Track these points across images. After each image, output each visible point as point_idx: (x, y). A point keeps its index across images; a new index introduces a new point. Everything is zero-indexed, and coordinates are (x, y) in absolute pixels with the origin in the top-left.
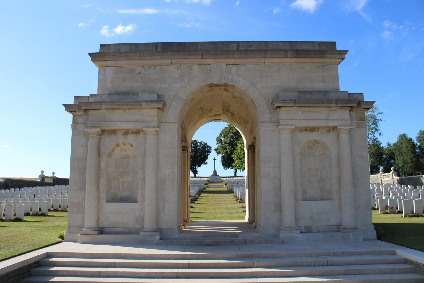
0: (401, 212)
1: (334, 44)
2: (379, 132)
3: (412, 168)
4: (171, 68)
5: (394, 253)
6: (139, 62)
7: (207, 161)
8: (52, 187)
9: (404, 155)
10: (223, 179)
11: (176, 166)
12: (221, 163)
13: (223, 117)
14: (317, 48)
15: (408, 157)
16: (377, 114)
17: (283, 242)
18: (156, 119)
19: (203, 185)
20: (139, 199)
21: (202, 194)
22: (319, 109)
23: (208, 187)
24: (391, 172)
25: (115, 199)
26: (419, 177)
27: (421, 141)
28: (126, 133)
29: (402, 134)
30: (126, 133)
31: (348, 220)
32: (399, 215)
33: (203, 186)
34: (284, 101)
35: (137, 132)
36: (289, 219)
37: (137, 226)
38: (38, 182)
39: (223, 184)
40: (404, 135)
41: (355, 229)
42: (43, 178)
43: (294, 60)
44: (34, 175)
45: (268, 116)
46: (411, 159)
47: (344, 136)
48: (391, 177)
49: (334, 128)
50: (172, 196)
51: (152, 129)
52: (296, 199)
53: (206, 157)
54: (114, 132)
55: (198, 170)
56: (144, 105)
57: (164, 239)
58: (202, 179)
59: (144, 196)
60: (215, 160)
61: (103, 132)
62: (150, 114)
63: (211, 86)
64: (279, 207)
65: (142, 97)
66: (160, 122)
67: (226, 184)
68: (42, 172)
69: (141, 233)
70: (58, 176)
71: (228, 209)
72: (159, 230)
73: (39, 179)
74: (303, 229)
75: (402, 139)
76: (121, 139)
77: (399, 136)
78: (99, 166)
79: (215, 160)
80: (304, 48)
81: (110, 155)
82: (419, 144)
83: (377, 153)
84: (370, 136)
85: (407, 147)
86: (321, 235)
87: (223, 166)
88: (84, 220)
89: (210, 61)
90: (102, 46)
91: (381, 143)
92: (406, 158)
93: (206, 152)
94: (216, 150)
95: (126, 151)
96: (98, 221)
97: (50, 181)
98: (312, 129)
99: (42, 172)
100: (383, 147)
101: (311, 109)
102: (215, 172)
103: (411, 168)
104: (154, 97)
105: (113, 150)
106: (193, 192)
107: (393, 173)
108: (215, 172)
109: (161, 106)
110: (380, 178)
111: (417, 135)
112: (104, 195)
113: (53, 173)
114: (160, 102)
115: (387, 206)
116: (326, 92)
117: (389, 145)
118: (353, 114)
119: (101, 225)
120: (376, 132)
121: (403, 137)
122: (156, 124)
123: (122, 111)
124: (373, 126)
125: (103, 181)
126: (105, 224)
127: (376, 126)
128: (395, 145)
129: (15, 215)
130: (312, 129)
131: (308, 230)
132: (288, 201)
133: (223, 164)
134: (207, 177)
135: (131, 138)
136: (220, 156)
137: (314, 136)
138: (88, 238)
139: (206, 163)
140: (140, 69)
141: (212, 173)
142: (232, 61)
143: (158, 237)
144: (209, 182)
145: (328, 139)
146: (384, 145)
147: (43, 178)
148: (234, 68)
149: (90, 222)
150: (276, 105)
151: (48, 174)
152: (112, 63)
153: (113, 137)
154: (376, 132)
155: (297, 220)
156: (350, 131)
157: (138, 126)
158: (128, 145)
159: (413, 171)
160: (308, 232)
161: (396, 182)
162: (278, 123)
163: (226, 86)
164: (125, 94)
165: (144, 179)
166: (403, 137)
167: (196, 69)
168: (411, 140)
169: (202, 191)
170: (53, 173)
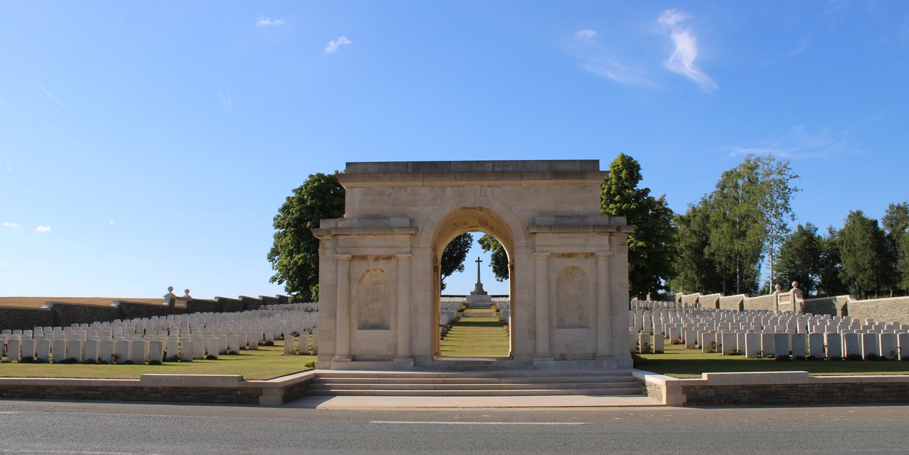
0: (700, 348)
1: (596, 163)
2: (790, 213)
3: (872, 280)
4: (424, 190)
5: (631, 374)
6: (389, 183)
7: (463, 263)
8: (186, 316)
9: (859, 254)
10: (493, 299)
11: (429, 293)
12: (491, 268)
13: (480, 228)
14: (578, 168)
15: (866, 258)
16: (788, 177)
17: (535, 369)
18: (408, 245)
19: (455, 312)
20: (392, 326)
21: (456, 329)
22: (576, 235)
23: (464, 316)
24: (792, 290)
25: (365, 327)
26: (831, 300)
27: (892, 226)
28: (377, 258)
29: (854, 211)
30: (377, 258)
31: (603, 348)
32: (698, 351)
33: (456, 314)
34: (539, 227)
35: (389, 258)
36: (543, 346)
37: (390, 353)
38: (164, 306)
39: (492, 310)
40: (859, 213)
41: (610, 357)
42: (172, 299)
43: (553, 181)
44: (155, 293)
45: (524, 241)
46: (872, 261)
47: (602, 263)
48: (791, 298)
49: (592, 254)
50: (424, 323)
51: (405, 256)
52: (550, 326)
53: (461, 256)
54: (364, 258)
55: (445, 282)
56: (396, 231)
57: (419, 365)
58: (453, 299)
59: (397, 323)
60: (479, 261)
61: (353, 257)
62: (401, 239)
63: (465, 208)
64: (533, 335)
65: (394, 221)
66: (412, 247)
67: (498, 311)
68: (171, 289)
69: (395, 360)
70: (194, 295)
71: (492, 346)
72: (412, 357)
73: (165, 301)
74: (557, 357)
75: (854, 222)
76: (372, 264)
77: (850, 216)
78: (350, 292)
79: (479, 261)
80: (564, 167)
81: (360, 281)
82: (887, 232)
83: (806, 250)
84: (773, 220)
85: (863, 238)
86: (574, 363)
87: (494, 274)
88: (335, 348)
89: (463, 183)
90: (348, 164)
91: (816, 229)
92: (860, 261)
93: (461, 246)
94: (481, 242)
95: (376, 276)
96: (350, 348)
97: (183, 305)
98: (570, 255)
99: (171, 289)
100: (819, 237)
101: (567, 235)
102: (479, 285)
103: (871, 279)
104: (406, 222)
105: (364, 276)
106: (444, 320)
107: (794, 292)
108: (479, 285)
109: (413, 232)
110: (775, 301)
111: (884, 214)
112: (355, 322)
113: (187, 291)
114: (412, 227)
115: (714, 343)
116: (585, 217)
117: (831, 231)
118: (614, 239)
119: (353, 353)
120: (785, 214)
121: (857, 218)
122: (408, 250)
123: (373, 237)
124: (779, 202)
125: (354, 308)
126: (357, 351)
127: (786, 202)
128: (842, 233)
129: (206, 353)
130: (570, 255)
131: (563, 358)
132: (542, 328)
133: (495, 270)
134: (464, 296)
135: (382, 264)
136: (490, 253)
137: (571, 262)
138: (342, 364)
139: (461, 269)
140: (390, 190)
141: (473, 289)
142: (487, 183)
143: (412, 363)
144: (467, 306)
145: (587, 265)
146: (823, 233)
147: (172, 299)
148: (489, 190)
149: (342, 349)
150: (532, 231)
151: (179, 293)
152: (361, 184)
153: (364, 263)
154: (785, 214)
155: (551, 347)
156: (609, 257)
157: (390, 252)
158: (379, 272)
159: (874, 285)
160: (563, 359)
161: (798, 308)
162: (533, 248)
163: (481, 208)
164: (375, 217)
165: (397, 306)
166: (857, 218)
167: (449, 191)
168: (875, 223)
169: (454, 322)
170: (187, 291)
